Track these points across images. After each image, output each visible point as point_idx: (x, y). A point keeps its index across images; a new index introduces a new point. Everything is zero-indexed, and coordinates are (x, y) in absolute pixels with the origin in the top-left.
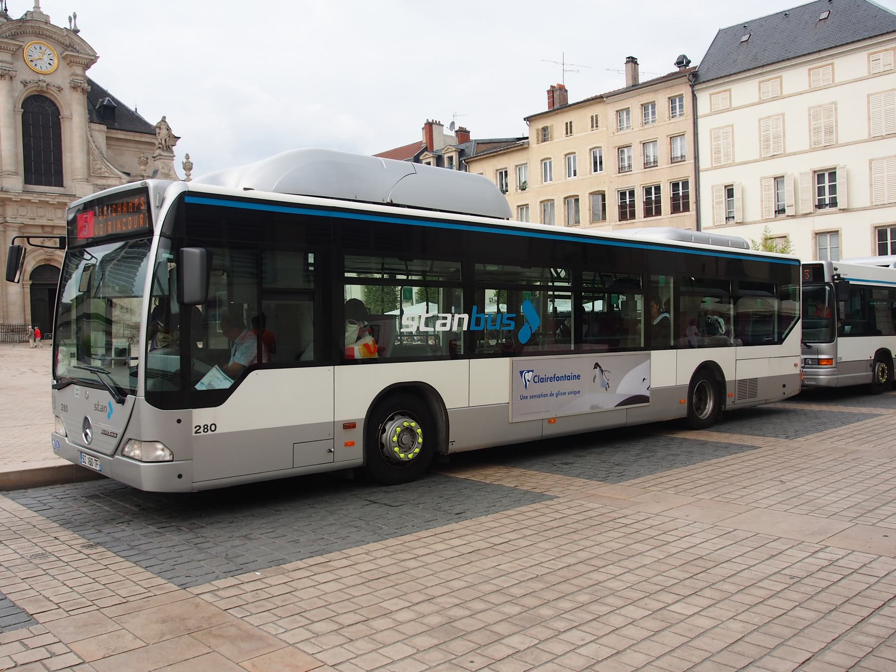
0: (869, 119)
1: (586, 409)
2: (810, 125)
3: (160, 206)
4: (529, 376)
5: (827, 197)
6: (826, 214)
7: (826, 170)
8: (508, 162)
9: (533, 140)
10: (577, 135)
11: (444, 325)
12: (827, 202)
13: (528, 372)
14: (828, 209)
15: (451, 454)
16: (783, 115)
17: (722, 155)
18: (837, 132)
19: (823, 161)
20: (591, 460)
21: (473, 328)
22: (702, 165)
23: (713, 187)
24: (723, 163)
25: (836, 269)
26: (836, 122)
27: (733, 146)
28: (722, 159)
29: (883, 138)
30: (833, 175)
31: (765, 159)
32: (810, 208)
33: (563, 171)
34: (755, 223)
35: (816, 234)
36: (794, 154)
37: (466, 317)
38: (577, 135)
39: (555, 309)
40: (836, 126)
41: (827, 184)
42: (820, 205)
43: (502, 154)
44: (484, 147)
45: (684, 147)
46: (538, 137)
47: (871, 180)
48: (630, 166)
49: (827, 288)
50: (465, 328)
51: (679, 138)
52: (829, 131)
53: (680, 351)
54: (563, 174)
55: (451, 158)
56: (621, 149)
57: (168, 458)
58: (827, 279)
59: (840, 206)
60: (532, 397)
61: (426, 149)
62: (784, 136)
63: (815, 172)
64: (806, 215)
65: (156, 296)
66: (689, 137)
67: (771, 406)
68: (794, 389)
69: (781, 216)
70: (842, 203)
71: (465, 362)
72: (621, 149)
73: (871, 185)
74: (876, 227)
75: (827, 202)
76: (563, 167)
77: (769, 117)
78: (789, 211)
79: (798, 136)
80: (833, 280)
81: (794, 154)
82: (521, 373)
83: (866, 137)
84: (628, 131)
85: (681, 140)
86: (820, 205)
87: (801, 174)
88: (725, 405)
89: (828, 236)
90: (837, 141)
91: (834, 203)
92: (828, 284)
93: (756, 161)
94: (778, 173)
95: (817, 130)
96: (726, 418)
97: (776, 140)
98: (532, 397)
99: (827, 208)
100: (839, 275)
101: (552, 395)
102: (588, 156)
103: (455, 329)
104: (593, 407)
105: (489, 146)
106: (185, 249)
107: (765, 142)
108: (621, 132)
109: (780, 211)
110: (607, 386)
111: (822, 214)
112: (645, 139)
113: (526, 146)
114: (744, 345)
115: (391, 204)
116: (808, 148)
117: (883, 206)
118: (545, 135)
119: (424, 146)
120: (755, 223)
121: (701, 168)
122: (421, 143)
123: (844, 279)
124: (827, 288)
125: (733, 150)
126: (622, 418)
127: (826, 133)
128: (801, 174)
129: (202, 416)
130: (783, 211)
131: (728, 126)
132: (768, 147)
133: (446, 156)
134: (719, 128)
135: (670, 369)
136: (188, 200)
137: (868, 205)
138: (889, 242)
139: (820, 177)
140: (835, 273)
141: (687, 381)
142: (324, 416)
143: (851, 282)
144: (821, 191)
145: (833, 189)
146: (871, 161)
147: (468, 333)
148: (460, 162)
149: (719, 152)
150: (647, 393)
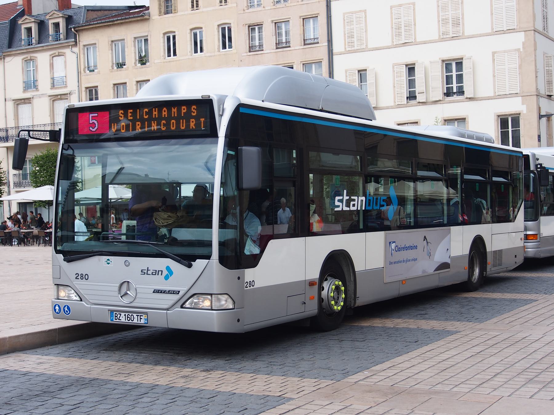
0: (492, 14)
1: (420, 274)
2: (438, 16)
3: (221, 116)
4: (393, 246)
5: (455, 86)
6: (454, 102)
7: (454, 60)
8: (128, 33)
9: (154, 11)
10: (205, 10)
11: (354, 205)
12: (455, 90)
13: (393, 242)
14: (455, 98)
15: (358, 307)
16: (414, 4)
17: (355, 39)
18: (463, 24)
19: (451, 51)
20: (452, 306)
21: (368, 208)
22: (337, 48)
23: (346, 71)
24: (356, 48)
25: (538, 159)
26: (463, 15)
27: (366, 31)
28: (356, 44)
29: (503, 32)
30: (459, 64)
31: (396, 46)
32: (438, 94)
33: (189, 46)
34: (388, 108)
35: (445, 120)
36: (425, 43)
37: (364, 198)
38: (205, 10)
39: (415, 191)
40: (463, 18)
41: (454, 74)
42: (448, 93)
43: (118, 24)
44: (94, 15)
45: (317, 30)
46: (160, 9)
47: (494, 71)
48: (261, 46)
49: (532, 175)
50: (364, 209)
51: (311, 20)
52: (457, 23)
53: (368, 234)
54: (189, 49)
55: (57, 25)
56: (251, 28)
57: (231, 307)
58: (532, 168)
59: (467, 94)
60: (395, 263)
61: (22, 14)
62: (415, 25)
63: (443, 61)
64: (436, 102)
65: (4, 184)
66: (322, 19)
67: (502, 275)
68: (520, 260)
69: (413, 102)
70: (468, 92)
71: (362, 234)
72: (251, 28)
73: (494, 76)
74: (498, 116)
75: (455, 90)
76: (189, 43)
77: (400, 5)
78: (420, 98)
79: (427, 26)
80: (537, 168)
81: (425, 43)
82: (390, 243)
83: (489, 31)
84: (260, 9)
85: (314, 21)
86: (448, 93)
87: (431, 62)
88: (486, 272)
89: (456, 123)
90: (463, 33)
91: (461, 92)
92: (532, 172)
93: (388, 48)
94: (410, 61)
95: (445, 21)
96: (488, 282)
97: (407, 28)
98: (395, 263)
99: (455, 96)
100: (541, 165)
101: (404, 261)
102: (216, 33)
103: (359, 209)
104: (424, 271)
105: (99, 13)
106: (243, 148)
107: (397, 30)
108: (251, 10)
109: (412, 97)
110: (429, 255)
111: (450, 102)
112: (276, 18)
113: (147, 17)
114: (493, 222)
115: (321, 111)
116: (437, 37)
117: (505, 96)
118: (167, 7)
119: (20, 8)
120: (388, 108)
121: (334, 51)
122: (15, 4)
123: (544, 168)
124: (532, 175)
125: (366, 35)
126: (434, 283)
127: (453, 25)
128: (431, 62)
129: (249, 274)
130: (415, 98)
131: (360, 11)
132: (399, 35)
133: (51, 22)
134: (352, 13)
135: (458, 241)
136: (242, 110)
137: (491, 94)
138: (510, 129)
139: (448, 67)
140: (537, 162)
141: (467, 251)
142: (301, 278)
143: (550, 171)
144: (449, 79)
145: (460, 78)
146: (494, 53)
147: (365, 211)
148: (68, 30)
149: (352, 37)
150: (449, 261)
